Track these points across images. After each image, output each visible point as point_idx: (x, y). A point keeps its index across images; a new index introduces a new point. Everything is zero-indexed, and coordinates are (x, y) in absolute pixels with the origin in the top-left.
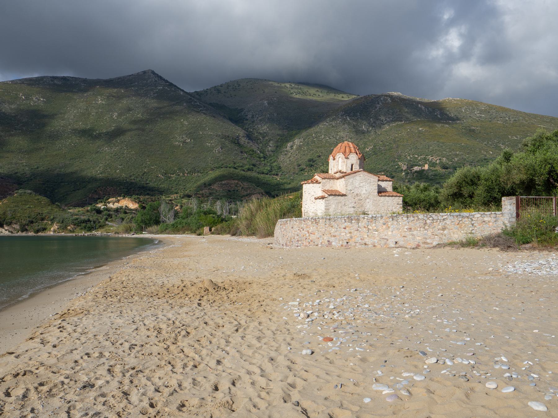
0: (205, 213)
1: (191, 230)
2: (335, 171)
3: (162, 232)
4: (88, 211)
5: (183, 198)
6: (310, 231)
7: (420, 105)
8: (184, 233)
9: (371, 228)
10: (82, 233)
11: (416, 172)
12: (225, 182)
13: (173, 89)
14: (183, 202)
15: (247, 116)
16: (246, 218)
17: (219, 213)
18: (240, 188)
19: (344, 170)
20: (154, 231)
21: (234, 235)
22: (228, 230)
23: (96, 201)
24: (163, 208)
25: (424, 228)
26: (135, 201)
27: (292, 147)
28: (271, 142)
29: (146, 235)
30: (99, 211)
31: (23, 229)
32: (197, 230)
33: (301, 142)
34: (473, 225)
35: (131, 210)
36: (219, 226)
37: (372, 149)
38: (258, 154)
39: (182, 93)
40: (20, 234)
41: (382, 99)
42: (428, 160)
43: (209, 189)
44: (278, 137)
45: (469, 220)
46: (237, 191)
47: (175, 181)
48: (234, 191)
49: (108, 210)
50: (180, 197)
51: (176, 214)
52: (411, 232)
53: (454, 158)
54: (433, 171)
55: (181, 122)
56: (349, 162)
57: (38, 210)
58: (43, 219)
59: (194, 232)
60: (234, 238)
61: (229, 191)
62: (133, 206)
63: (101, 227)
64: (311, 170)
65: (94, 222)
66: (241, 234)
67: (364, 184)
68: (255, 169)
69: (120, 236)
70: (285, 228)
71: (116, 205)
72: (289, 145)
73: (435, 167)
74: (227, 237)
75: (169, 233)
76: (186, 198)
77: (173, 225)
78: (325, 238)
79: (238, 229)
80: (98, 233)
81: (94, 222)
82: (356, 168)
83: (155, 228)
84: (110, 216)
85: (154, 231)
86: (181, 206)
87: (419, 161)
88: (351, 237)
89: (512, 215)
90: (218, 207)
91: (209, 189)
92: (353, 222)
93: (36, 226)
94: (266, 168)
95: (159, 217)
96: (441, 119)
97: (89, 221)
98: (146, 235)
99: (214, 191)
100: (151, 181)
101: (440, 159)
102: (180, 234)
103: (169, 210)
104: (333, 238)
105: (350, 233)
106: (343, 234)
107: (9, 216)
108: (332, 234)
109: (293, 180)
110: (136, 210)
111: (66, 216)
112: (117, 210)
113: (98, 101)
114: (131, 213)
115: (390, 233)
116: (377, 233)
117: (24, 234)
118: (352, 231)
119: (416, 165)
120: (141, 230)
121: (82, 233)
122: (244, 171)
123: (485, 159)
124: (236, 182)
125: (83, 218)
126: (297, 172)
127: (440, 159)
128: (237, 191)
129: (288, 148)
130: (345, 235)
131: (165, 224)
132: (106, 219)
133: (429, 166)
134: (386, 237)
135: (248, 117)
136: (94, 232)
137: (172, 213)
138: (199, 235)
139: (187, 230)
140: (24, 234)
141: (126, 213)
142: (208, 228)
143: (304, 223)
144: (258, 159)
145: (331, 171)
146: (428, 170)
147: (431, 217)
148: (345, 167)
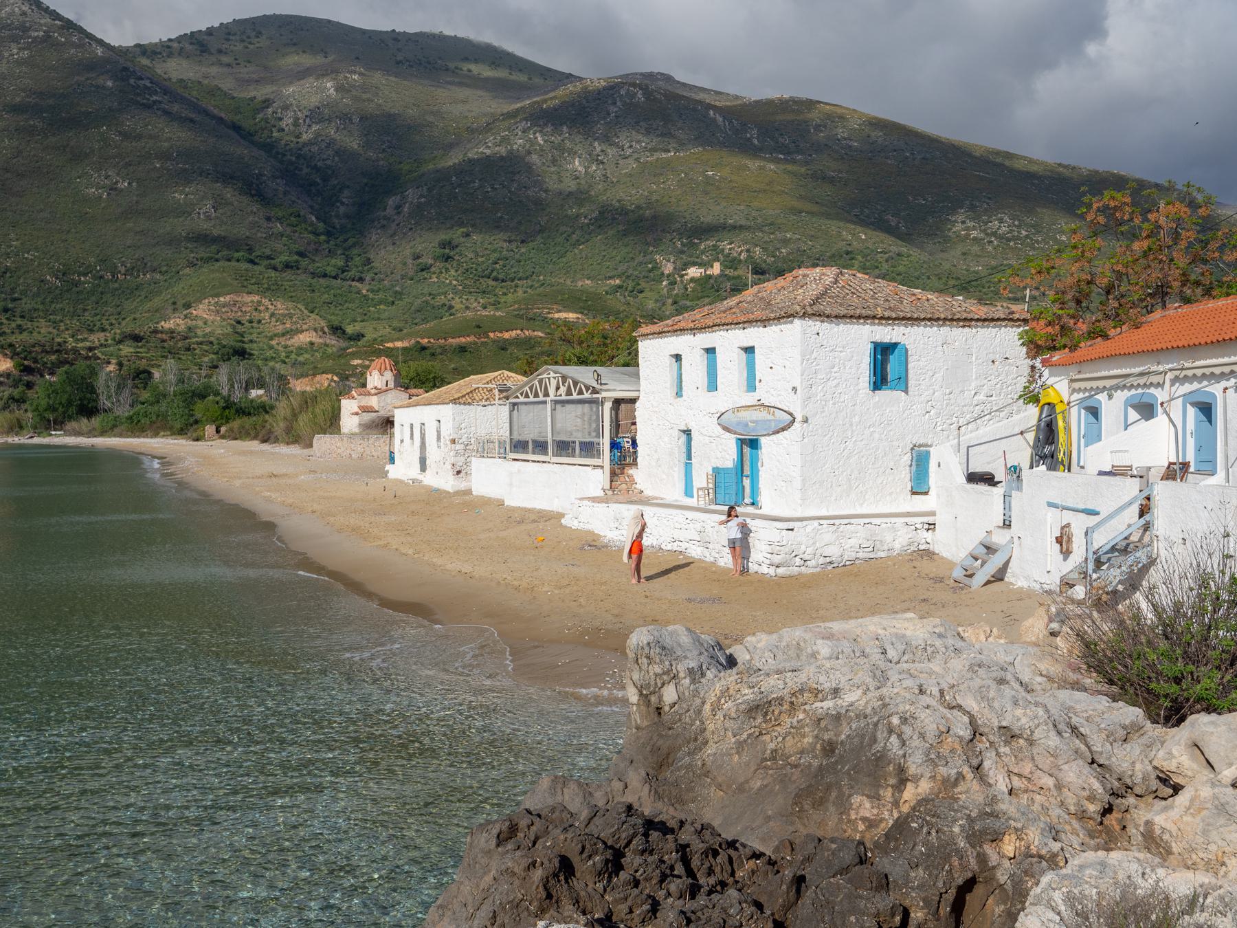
1: (171, 428)
3: (103, 433)
5: (120, 342)
7: (711, 112)
8: (156, 435)
11: (692, 280)
12: (228, 298)
13: (75, 39)
14: (123, 353)
15: (281, 119)
16: (285, 418)
17: (225, 392)
18: (267, 315)
20: (85, 429)
21: (264, 441)
22: (253, 433)
27: (398, 208)
28: (346, 193)
33: (422, 196)
37: (596, 219)
38: (312, 224)
39: (99, 51)
41: (623, 92)
42: (723, 250)
43: (186, 316)
44: (365, 181)
46: (259, 322)
47: (92, 292)
48: (251, 322)
50: (114, 339)
53: (778, 249)
54: (729, 278)
56: (384, 379)
60: (266, 447)
61: (239, 322)
64: (447, 270)
66: (276, 441)
68: (304, 263)
70: (322, 443)
72: (392, 201)
73: (736, 269)
74: (254, 445)
75: (121, 436)
76: (130, 342)
77: (130, 418)
79: (270, 432)
82: (391, 385)
85: (85, 429)
86: (120, 365)
87: (703, 252)
91: (186, 316)
94: (333, 261)
96: (761, 150)
99: (200, 323)
100: (24, 293)
101: (748, 251)
102: (146, 436)
109: (401, 293)
119: (694, 264)
122: (275, 268)
123: (848, 253)
124: (256, 298)
126: (411, 274)
127: (748, 251)
128: (259, 322)
129: (390, 211)
130: (360, 449)
131: (111, 416)
133: (724, 266)
135: (283, 124)
138: (197, 440)
139: (164, 428)
142: (214, 427)
144: (312, 237)
145: (370, 386)
146: (720, 276)
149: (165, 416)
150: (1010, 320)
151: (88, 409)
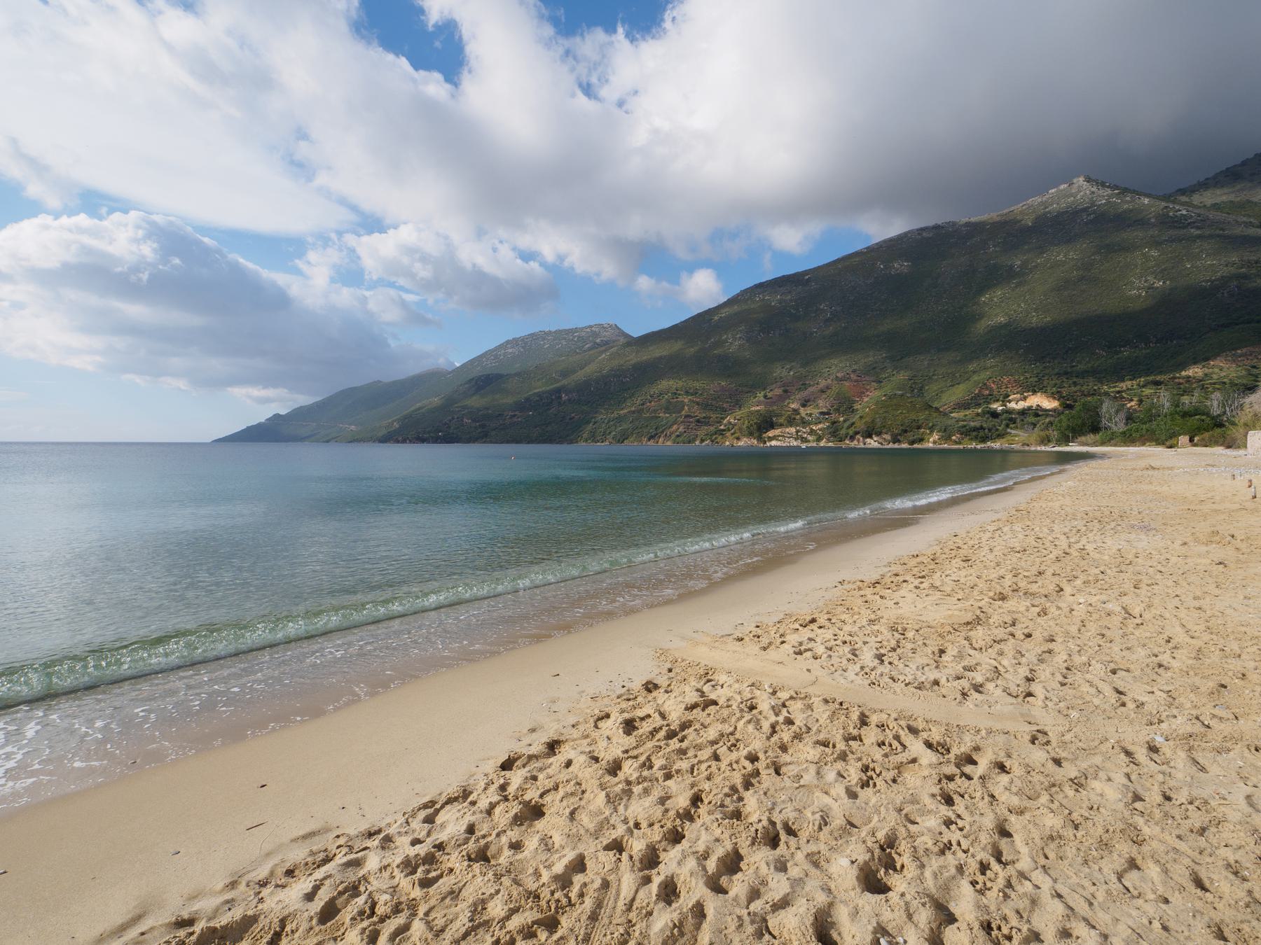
0: (1186, 415)
3: (1103, 444)
4: (978, 414)
5: (1144, 386)
8: (1143, 444)
10: (973, 445)
12: (1244, 350)
21: (1229, 447)
23: (992, 398)
24: (1107, 407)
26: (1053, 396)
29: (1074, 448)
30: (995, 415)
31: (895, 440)
32: (1167, 440)
35: (1046, 410)
36: (1207, 435)
40: (891, 446)
49: (1009, 412)
51: (1130, 418)
55: (1144, 254)
57: (913, 416)
58: (919, 428)
59: (1159, 442)
60: (1229, 452)
62: (1048, 404)
63: (1001, 436)
65: (990, 430)
69: (1033, 449)
71: (1021, 405)
74: (1219, 450)
77: (1124, 433)
80: (996, 445)
81: (990, 430)
83: (1091, 437)
84: (1013, 421)
86: (1141, 401)
90: (1215, 403)
93: (910, 436)
95: (1100, 422)
97: (982, 428)
98: (1074, 448)
103: (1117, 412)
107: (879, 424)
110: (1054, 410)
111: (950, 422)
112: (1023, 412)
114: (1047, 415)
117: (896, 446)
120: (1066, 440)
121: (973, 445)
125: (972, 424)
132: (1007, 426)
136: (989, 444)
137: (1122, 415)
138: (1171, 447)
140: (896, 446)
141: (1037, 415)
142: (1187, 438)
149: (1153, 432)
150: (1246, 436)
151: (1095, 429)
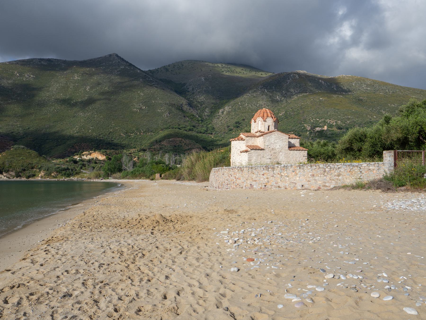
0: (157, 163)
1: (146, 176)
2: (256, 131)
3: (123, 178)
4: (67, 162)
5: (139, 151)
6: (237, 177)
7: (320, 81)
8: (140, 178)
9: (283, 174)
10: (63, 179)
11: (318, 131)
12: (172, 139)
13: (132, 68)
14: (140, 155)
15: (188, 89)
16: (188, 167)
17: (167, 163)
18: (184, 144)
19: (263, 130)
20: (118, 176)
21: (178, 180)
22: (174, 176)
23: (73, 154)
24: (125, 159)
25: (324, 174)
26: (103, 154)
27: (223, 112)
28: (207, 109)
29: (111, 180)
30: (75, 162)
31: (18, 176)
32: (150, 176)
33: (230, 109)
34: (361, 172)
35: (100, 161)
36: (167, 173)
37: (284, 114)
38: (197, 118)
39: (139, 71)
40: (15, 179)
41: (291, 76)
42: (327, 122)
43: (160, 145)
44: (213, 105)
45: (358, 168)
46: (181, 146)
47: (134, 138)
48: (178, 146)
49: (82, 160)
50: (137, 151)
51: (135, 164)
52: (314, 178)
53: (346, 121)
54: (330, 131)
55: (138, 94)
56: (267, 124)
57: (29, 161)
58: (33, 168)
59: (148, 177)
60: (179, 182)
61: (175, 146)
62: (101, 157)
63: (77, 173)
64: (238, 130)
65: (72, 170)
66: (184, 179)
67: (278, 141)
68: (195, 129)
69: (92, 181)
70: (218, 175)
71: (89, 157)
72: (221, 111)
73: (332, 128)
74: (174, 181)
75: (129, 179)
76: (142, 152)
77: (132, 172)
78: (248, 182)
79: (181, 175)
80: (75, 178)
81: (72, 170)
82: (272, 128)
83: (118, 174)
84: (84, 165)
85: (118, 176)
86: (139, 158)
87: (320, 123)
88: (268, 182)
89: (391, 164)
90: (167, 159)
91: (160, 145)
92: (269, 170)
93: (27, 173)
94: (203, 129)
95: (122, 166)
96: (337, 91)
97: (68, 169)
98: (111, 180)
99: (164, 147)
100: (115, 139)
101: (336, 122)
102: (137, 179)
103: (129, 161)
104: (254, 182)
105: (267, 178)
106: (262, 179)
107: (7, 166)
108: (254, 179)
109: (224, 137)
110: (104, 160)
111: (50, 165)
112: (89, 161)
113: (75, 77)
114: (100, 163)
115: (298, 178)
116: (287, 178)
117: (18, 179)
118: (269, 177)
119: (318, 127)
120: (107, 176)
121: (63, 179)
122: (186, 131)
123: (370, 122)
124: (180, 139)
125: (63, 167)
126: (226, 132)
127: (336, 122)
128: (181, 146)
129: (220, 113)
130: (263, 180)
131: (126, 172)
132: (81, 168)
133: (328, 127)
134: (295, 182)
135: (189, 90)
136: (72, 178)
137: (131, 163)
138: (152, 180)
139: (143, 176)
140: (18, 179)
141: (96, 163)
142: (159, 175)
143: (232, 170)
144: (197, 122)
145: (253, 131)
146: (327, 130)
147: (329, 166)
148: (263, 128)
